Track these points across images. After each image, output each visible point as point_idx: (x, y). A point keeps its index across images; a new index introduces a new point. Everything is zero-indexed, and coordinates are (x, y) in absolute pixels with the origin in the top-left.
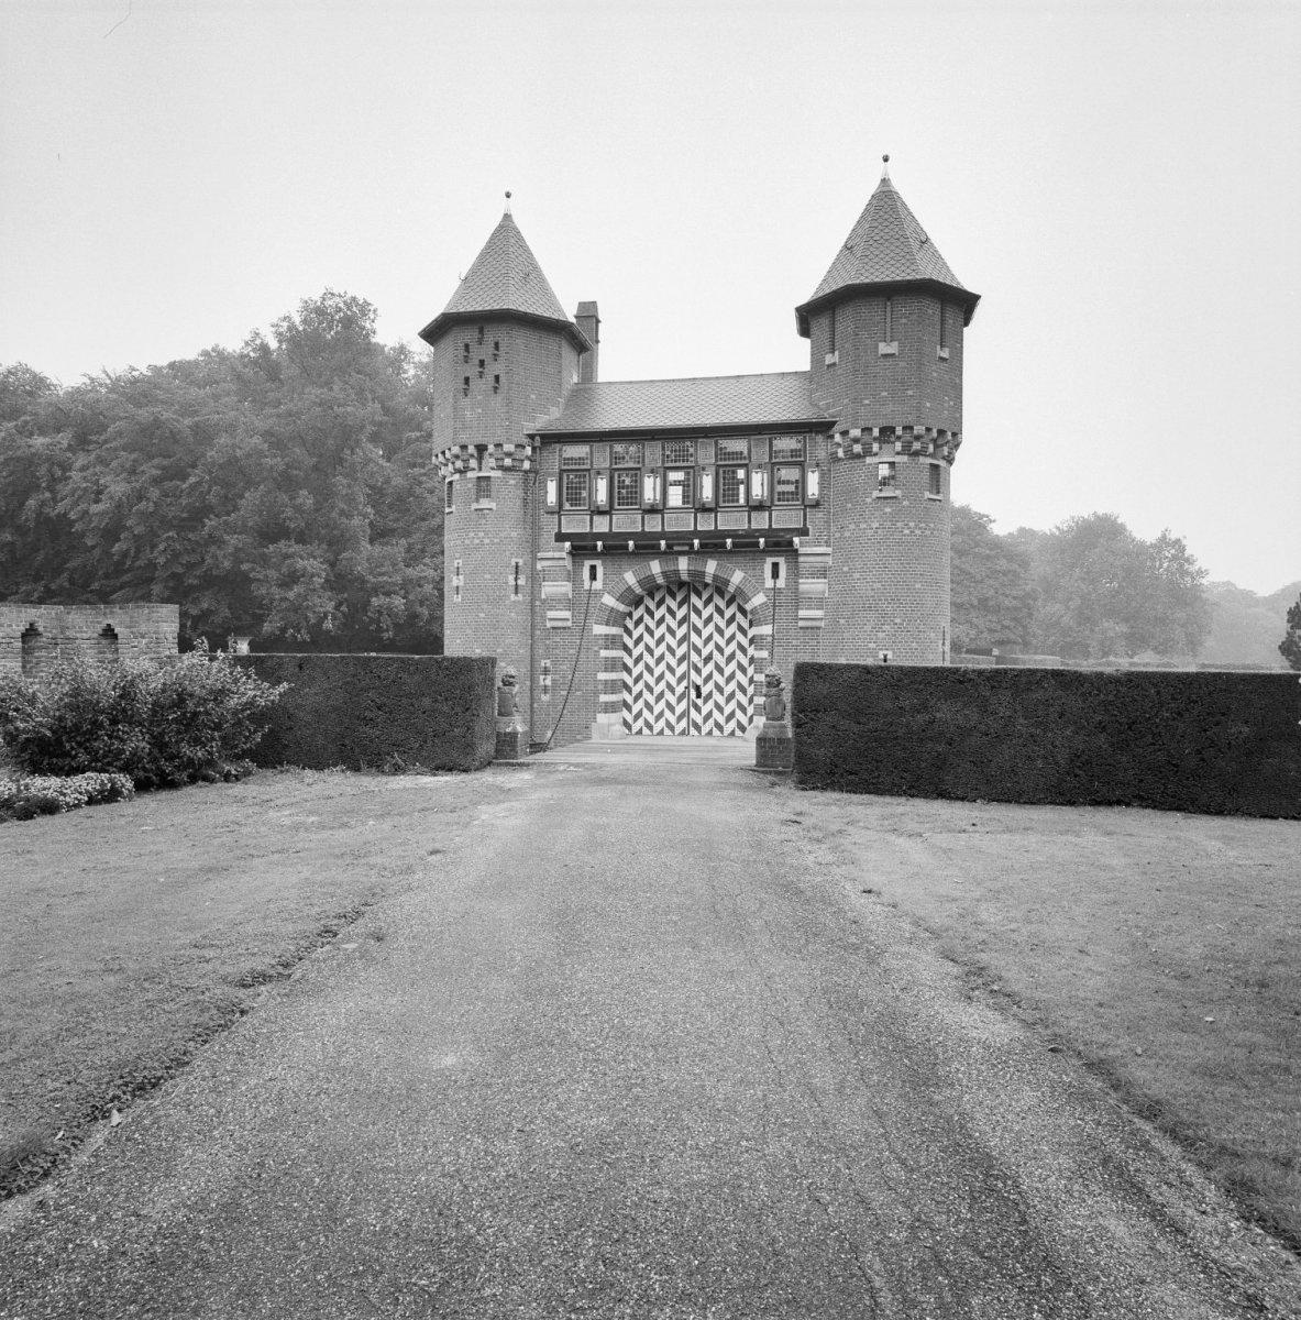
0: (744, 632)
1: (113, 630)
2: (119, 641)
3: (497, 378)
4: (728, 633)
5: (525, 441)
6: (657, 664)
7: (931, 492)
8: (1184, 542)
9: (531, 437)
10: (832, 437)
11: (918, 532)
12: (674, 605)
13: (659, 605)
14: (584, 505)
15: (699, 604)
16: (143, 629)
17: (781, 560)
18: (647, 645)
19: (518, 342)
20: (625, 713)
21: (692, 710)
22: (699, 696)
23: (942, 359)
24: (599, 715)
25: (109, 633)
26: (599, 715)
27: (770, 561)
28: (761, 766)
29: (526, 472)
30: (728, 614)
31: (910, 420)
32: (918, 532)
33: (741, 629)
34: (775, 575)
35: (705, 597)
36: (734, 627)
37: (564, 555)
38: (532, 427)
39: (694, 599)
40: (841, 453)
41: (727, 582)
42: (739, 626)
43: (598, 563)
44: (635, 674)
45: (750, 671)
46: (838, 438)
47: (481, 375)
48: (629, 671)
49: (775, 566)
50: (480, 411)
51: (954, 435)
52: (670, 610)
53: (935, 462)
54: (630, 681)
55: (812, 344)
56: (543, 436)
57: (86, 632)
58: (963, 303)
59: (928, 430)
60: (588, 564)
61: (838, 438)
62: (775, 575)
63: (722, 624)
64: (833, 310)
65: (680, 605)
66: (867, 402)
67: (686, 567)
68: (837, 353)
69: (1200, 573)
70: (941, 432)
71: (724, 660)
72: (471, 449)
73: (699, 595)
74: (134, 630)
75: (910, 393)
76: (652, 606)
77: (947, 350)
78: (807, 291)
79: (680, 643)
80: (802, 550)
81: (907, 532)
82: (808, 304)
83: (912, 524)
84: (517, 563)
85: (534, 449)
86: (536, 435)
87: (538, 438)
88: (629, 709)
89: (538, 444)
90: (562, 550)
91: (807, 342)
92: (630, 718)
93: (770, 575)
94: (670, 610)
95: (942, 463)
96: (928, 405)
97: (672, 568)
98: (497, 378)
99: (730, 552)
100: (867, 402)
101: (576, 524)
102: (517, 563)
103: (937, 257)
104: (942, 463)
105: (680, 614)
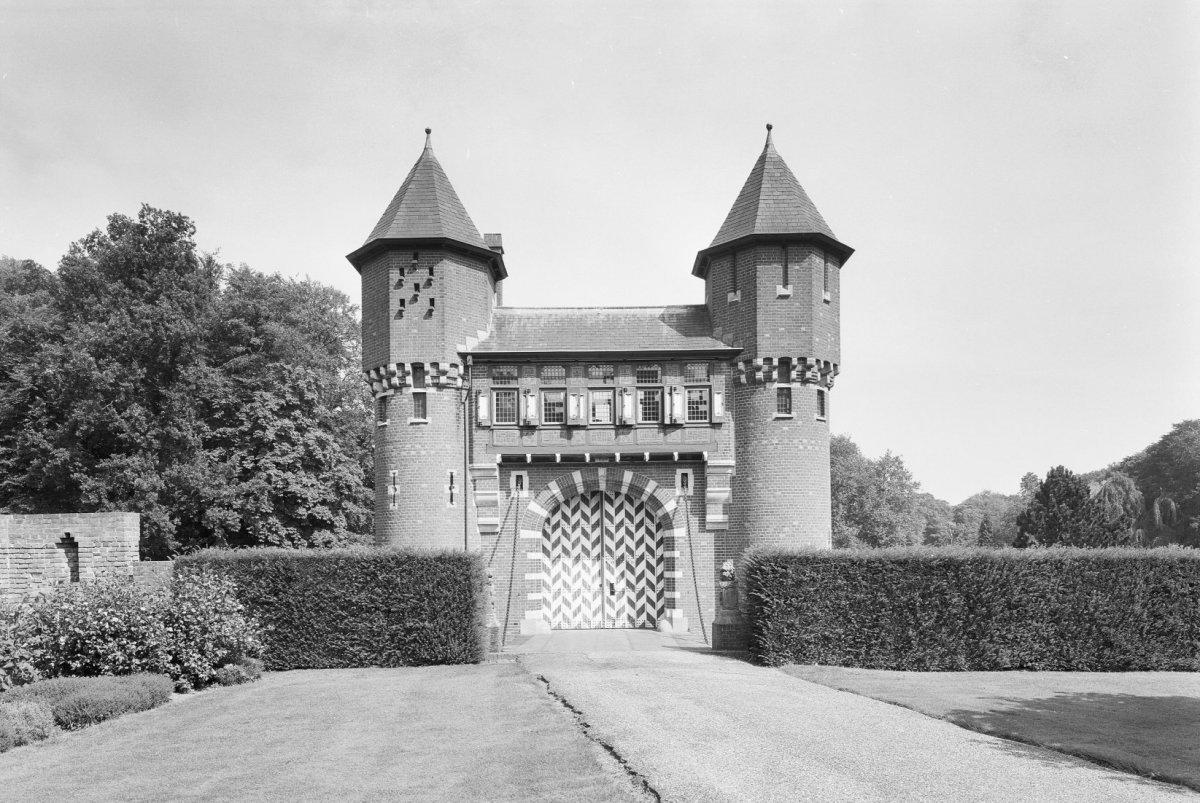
0: (652, 535)
1: (73, 538)
2: (80, 550)
3: (432, 301)
4: (638, 536)
5: (458, 361)
6: (638, 563)
7: (416, 416)
8: (901, 459)
9: (463, 356)
10: (737, 365)
11: (809, 447)
12: (588, 511)
13: (574, 511)
14: (705, 418)
15: (611, 511)
16: (107, 536)
17: (689, 471)
18: (583, 547)
19: (450, 269)
20: (545, 609)
21: (607, 606)
22: (612, 593)
23: (826, 302)
24: (527, 613)
25: (69, 543)
26: (527, 613)
27: (679, 472)
28: (718, 649)
29: (458, 389)
30: (637, 519)
31: (803, 353)
32: (809, 447)
33: (649, 532)
34: (684, 484)
35: (593, 504)
36: (642, 531)
37: (495, 466)
38: (471, 346)
39: (607, 506)
40: (743, 379)
41: (641, 492)
42: (647, 529)
43: (524, 473)
44: (553, 574)
45: (659, 570)
46: (741, 366)
47: (415, 299)
48: (548, 571)
49: (685, 475)
50: (416, 331)
51: (835, 365)
52: (584, 516)
53: (821, 388)
54: (549, 581)
55: (706, 285)
56: (475, 356)
57: (40, 541)
58: (839, 253)
59: (818, 361)
60: (514, 474)
61: (741, 366)
62: (684, 484)
63: (632, 529)
64: (734, 255)
65: (593, 511)
66: (768, 335)
67: (629, 481)
68: (739, 292)
69: (916, 485)
70: (827, 363)
71: (634, 560)
72: (408, 368)
73: (611, 502)
74: (98, 538)
75: (803, 329)
76: (568, 512)
77: (829, 294)
78: (358, 242)
79: (594, 545)
80: (710, 463)
81: (801, 447)
82: (706, 250)
83: (805, 441)
84: (452, 473)
85: (466, 367)
86: (468, 354)
87: (469, 358)
88: (548, 605)
89: (470, 363)
90: (493, 460)
91: (702, 282)
92: (550, 614)
93: (680, 484)
94: (584, 516)
95: (825, 389)
96: (817, 340)
97: (593, 478)
98: (432, 301)
99: (559, 465)
100: (768, 335)
101: (513, 441)
102: (452, 473)
103: (461, 213)
104: (825, 389)
105: (594, 519)
